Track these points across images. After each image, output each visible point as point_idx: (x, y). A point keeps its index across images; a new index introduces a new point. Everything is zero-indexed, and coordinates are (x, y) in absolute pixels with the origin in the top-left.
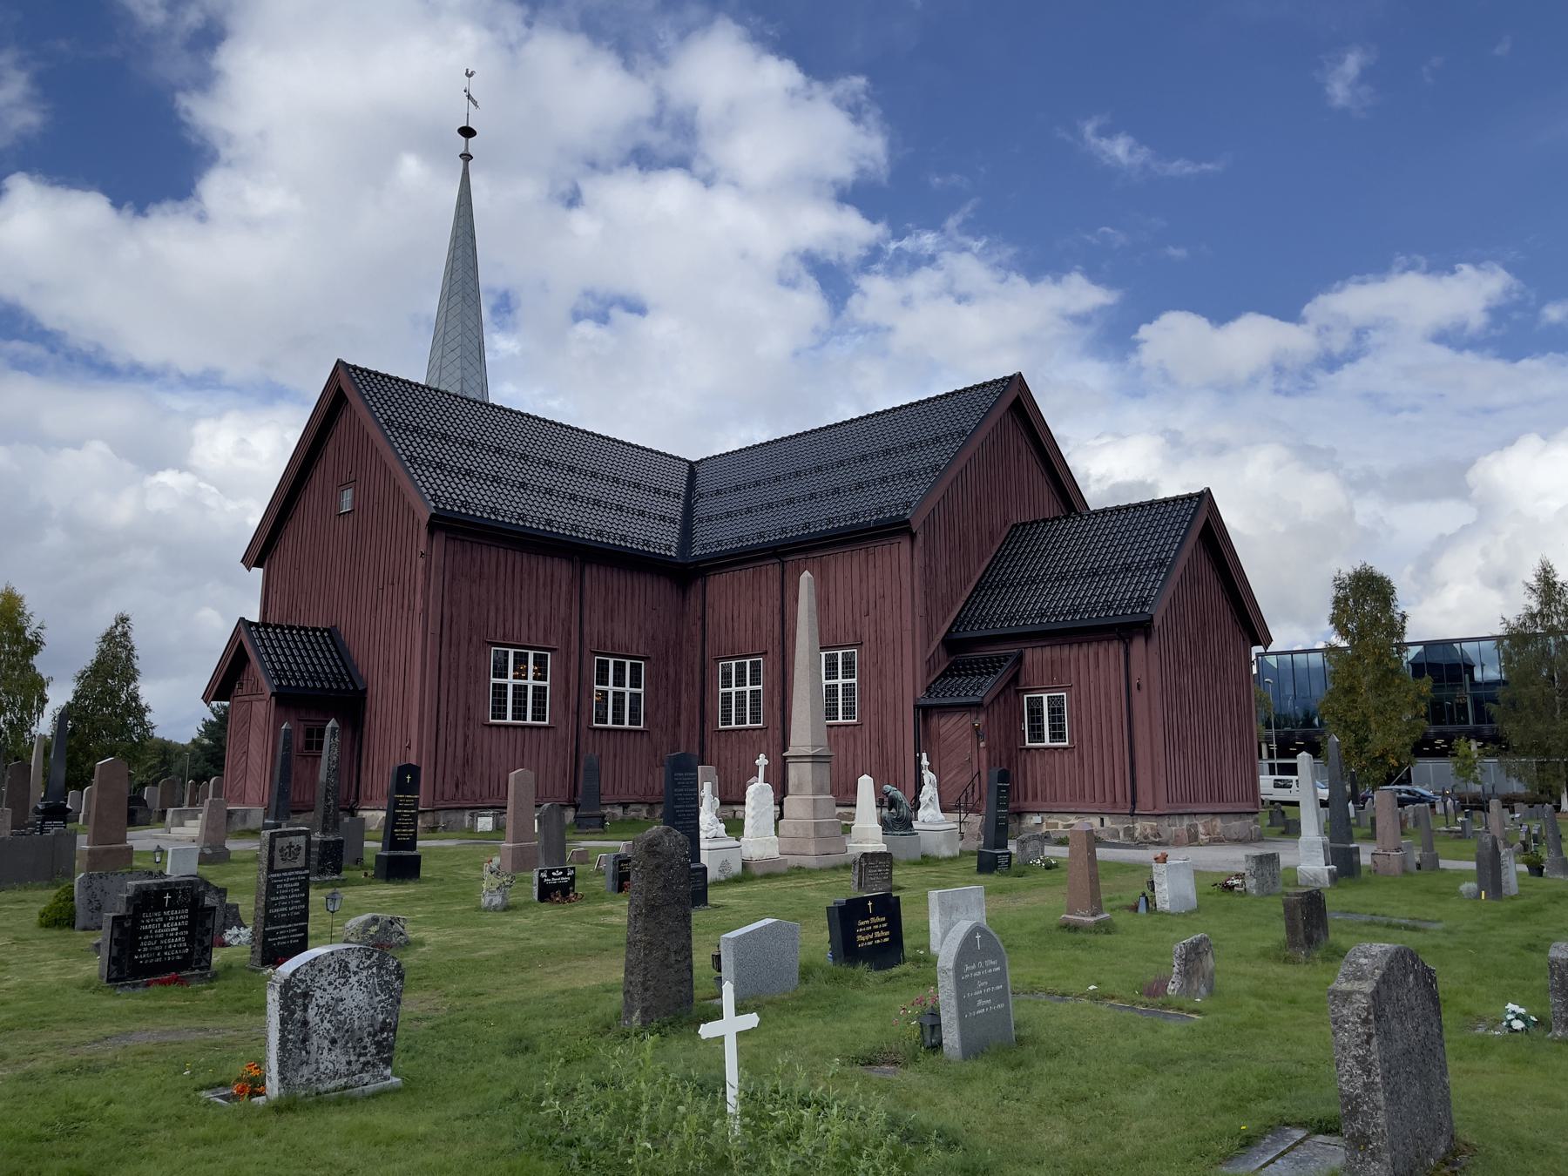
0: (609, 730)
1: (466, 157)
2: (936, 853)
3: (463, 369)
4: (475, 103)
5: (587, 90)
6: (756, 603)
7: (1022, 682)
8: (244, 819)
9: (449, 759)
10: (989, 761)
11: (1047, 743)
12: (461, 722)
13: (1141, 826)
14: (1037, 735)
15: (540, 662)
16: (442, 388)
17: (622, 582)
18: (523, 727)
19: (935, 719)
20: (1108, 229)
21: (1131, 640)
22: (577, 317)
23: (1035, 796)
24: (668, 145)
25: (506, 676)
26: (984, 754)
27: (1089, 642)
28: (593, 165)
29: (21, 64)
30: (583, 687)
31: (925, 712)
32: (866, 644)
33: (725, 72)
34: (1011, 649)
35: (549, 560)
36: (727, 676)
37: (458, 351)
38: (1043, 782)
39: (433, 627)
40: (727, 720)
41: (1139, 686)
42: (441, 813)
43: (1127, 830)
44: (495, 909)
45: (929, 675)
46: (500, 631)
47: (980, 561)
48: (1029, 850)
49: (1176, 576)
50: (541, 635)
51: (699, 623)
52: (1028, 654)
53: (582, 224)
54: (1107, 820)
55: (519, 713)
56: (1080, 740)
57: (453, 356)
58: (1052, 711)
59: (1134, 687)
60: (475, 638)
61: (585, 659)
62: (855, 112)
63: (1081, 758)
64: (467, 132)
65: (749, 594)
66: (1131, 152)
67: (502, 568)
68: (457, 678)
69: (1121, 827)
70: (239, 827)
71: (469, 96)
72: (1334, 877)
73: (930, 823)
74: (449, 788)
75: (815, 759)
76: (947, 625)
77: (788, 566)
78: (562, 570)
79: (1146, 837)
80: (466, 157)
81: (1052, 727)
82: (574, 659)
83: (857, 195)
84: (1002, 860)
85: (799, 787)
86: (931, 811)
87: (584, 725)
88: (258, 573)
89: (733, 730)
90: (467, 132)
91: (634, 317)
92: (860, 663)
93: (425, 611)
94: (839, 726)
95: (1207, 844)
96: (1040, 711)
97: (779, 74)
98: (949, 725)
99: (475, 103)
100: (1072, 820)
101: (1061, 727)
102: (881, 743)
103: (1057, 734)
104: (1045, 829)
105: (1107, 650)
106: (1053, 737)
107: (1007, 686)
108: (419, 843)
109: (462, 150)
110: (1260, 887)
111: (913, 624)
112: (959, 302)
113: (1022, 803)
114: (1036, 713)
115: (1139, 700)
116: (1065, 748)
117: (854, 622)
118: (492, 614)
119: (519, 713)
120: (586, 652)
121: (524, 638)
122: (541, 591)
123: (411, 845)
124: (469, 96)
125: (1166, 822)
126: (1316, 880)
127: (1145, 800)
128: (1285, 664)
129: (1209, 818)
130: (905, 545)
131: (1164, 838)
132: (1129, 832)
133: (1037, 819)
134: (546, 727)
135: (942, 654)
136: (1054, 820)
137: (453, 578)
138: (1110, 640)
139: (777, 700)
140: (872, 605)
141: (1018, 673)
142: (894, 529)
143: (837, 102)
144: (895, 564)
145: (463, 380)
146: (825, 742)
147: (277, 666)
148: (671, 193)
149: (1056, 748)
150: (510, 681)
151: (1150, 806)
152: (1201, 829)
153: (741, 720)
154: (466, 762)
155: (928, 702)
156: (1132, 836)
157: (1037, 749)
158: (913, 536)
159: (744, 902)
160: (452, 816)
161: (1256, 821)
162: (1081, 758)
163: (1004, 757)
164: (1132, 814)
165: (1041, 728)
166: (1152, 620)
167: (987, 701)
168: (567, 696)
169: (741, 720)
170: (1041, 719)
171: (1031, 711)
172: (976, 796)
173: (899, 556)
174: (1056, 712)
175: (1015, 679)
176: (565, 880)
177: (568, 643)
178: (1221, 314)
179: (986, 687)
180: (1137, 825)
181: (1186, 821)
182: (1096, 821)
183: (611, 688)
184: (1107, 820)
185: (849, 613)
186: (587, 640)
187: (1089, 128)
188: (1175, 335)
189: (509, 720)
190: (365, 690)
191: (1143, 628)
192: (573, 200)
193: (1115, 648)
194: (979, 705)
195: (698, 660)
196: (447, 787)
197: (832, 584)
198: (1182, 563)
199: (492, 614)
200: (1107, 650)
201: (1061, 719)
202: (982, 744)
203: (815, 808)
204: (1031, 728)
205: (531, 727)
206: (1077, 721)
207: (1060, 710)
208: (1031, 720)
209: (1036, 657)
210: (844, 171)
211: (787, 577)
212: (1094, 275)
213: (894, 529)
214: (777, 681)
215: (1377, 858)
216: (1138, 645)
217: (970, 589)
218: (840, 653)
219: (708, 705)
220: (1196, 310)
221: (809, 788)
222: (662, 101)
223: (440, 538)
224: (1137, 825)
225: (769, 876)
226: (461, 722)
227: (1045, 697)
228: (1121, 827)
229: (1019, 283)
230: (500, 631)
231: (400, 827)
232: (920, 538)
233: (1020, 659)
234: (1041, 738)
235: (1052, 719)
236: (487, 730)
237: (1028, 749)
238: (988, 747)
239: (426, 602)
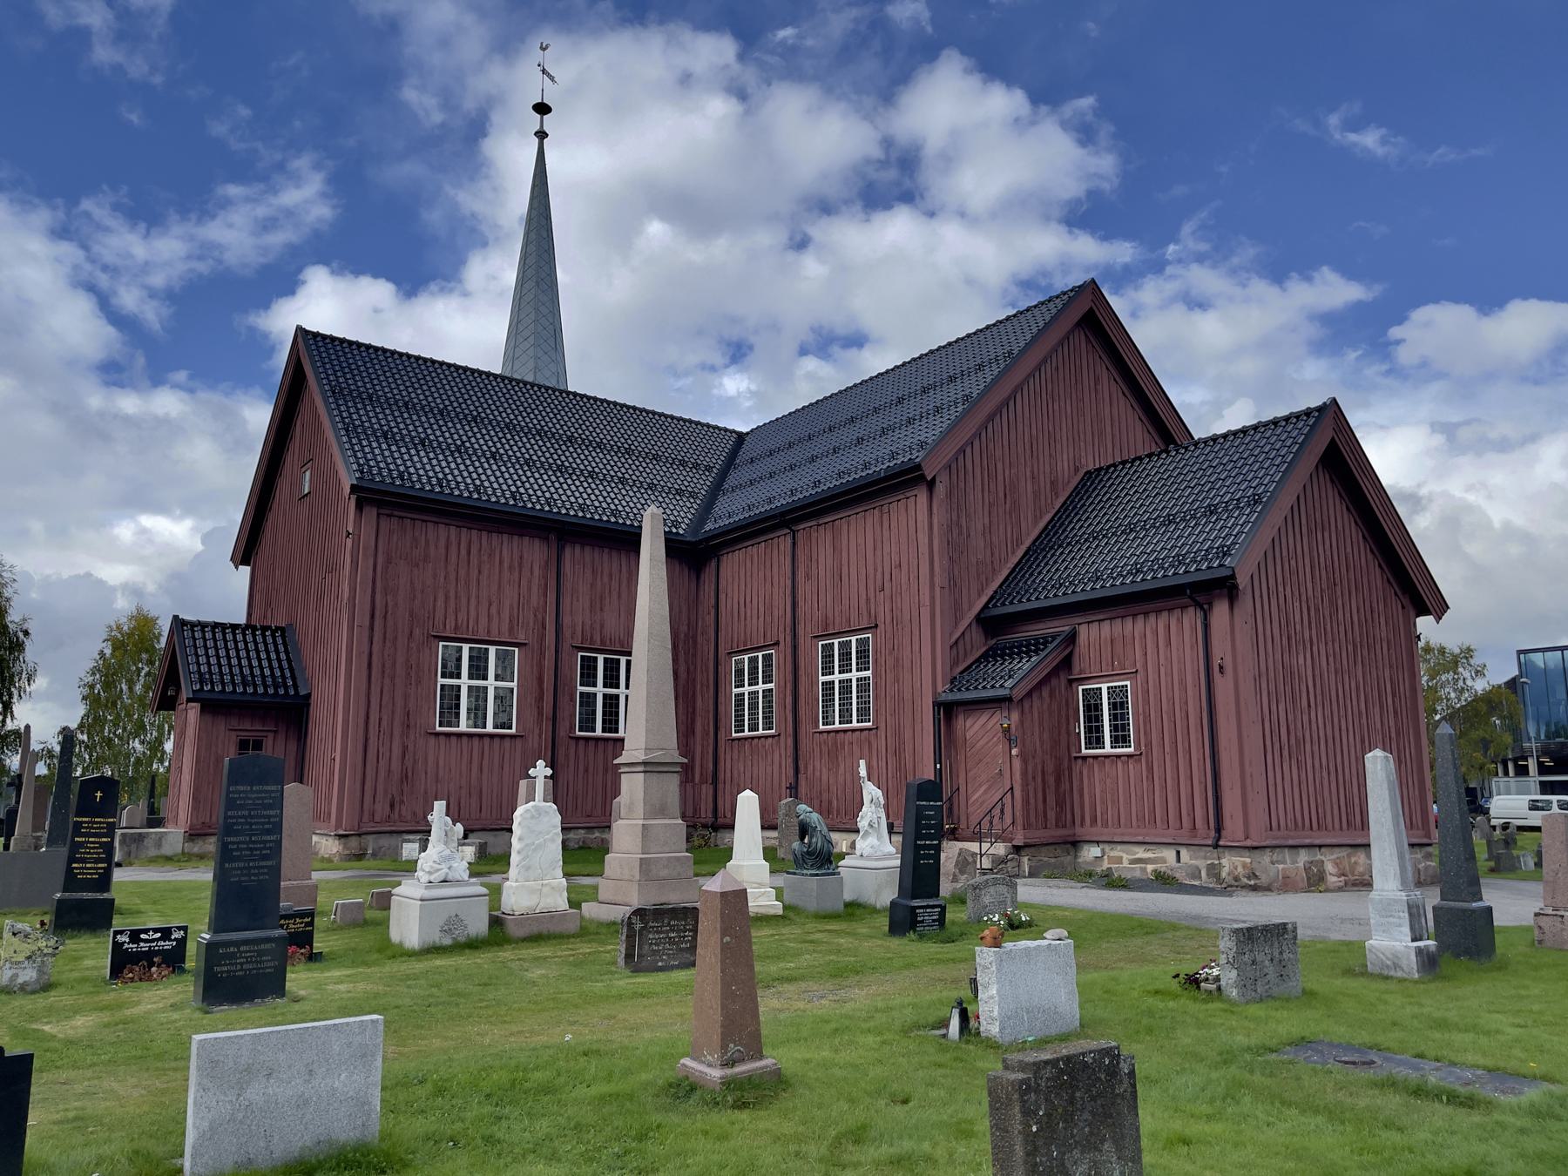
0: (597, 739)
1: (542, 135)
2: (872, 901)
3: (537, 358)
4: (552, 78)
5: (820, 135)
6: (768, 585)
7: (1076, 669)
8: (159, 844)
9: (382, 774)
10: (1024, 773)
11: (1108, 749)
12: (397, 732)
13: (1232, 863)
14: (1095, 739)
15: (503, 659)
16: (516, 376)
17: (615, 565)
18: (481, 736)
19: (961, 718)
20: (1362, 224)
21: (1210, 604)
22: (803, 351)
23: (1094, 821)
24: (894, 181)
25: (459, 676)
26: (1017, 764)
27: (1158, 611)
28: (826, 208)
29: (317, 167)
30: (560, 686)
31: (947, 711)
32: (881, 626)
33: (950, 105)
34: (1061, 626)
35: (614, 554)
36: (740, 672)
37: (531, 340)
38: (1104, 802)
39: (362, 618)
40: (740, 729)
41: (1221, 667)
42: (370, 838)
43: (1211, 867)
44: (23, 988)
45: (955, 663)
46: (450, 624)
47: (1036, 523)
48: (987, 900)
49: (1276, 517)
50: (505, 627)
51: (713, 612)
52: (1083, 631)
53: (812, 267)
54: (1184, 852)
55: (477, 713)
56: (1149, 744)
57: (527, 344)
58: (1113, 706)
59: (1216, 669)
60: (417, 631)
61: (564, 656)
62: (1085, 134)
63: (1150, 769)
64: (542, 109)
65: (761, 574)
66: (1384, 141)
67: (454, 549)
68: (393, 678)
69: (1202, 864)
70: (153, 852)
71: (544, 71)
72: (1429, 962)
73: (869, 858)
74: (381, 808)
75: (649, 767)
76: (984, 599)
77: (799, 535)
78: (535, 552)
79: (1236, 879)
80: (542, 135)
81: (1114, 728)
82: (550, 654)
83: (1085, 215)
84: (927, 916)
85: (630, 808)
86: (872, 840)
87: (562, 732)
88: (246, 570)
89: (746, 739)
90: (542, 109)
91: (853, 352)
92: (876, 652)
93: (352, 598)
94: (853, 731)
95: (1340, 889)
96: (1098, 707)
97: (1003, 102)
98: (977, 727)
99: (552, 78)
100: (1141, 853)
101: (1125, 727)
102: (898, 753)
103: (1120, 739)
104: (1106, 865)
105: (1180, 621)
106: (1116, 741)
107: (1054, 672)
108: (118, 875)
109: (537, 128)
110: (1242, 985)
111: (932, 598)
112: (1191, 309)
113: (1078, 830)
114: (1093, 709)
115: (1223, 686)
116: (1130, 756)
117: (868, 600)
118: (440, 603)
119: (477, 713)
120: (566, 646)
121: (495, 631)
122: (506, 574)
123: (104, 882)
124: (544, 71)
125: (1266, 858)
126: (1396, 966)
127: (1233, 825)
128: (1551, 665)
129: (1343, 853)
130: (922, 495)
131: (1264, 880)
132: (1214, 871)
133: (1095, 851)
134: (512, 736)
135: (977, 635)
136: (1117, 852)
137: (389, 561)
138: (1183, 608)
139: (789, 700)
140: (887, 577)
141: (1070, 655)
142: (906, 479)
143: (1065, 125)
144: (912, 523)
145: (536, 369)
146: (672, 742)
147: (204, 669)
148: (897, 229)
149: (1119, 756)
150: (464, 682)
151: (1240, 834)
152: (1330, 867)
153: (754, 727)
154: (405, 777)
155: (951, 697)
156: (1217, 876)
157: (1095, 757)
158: (931, 485)
159: (176, 1016)
160: (385, 841)
161: (1428, 856)
162: (1150, 769)
163: (1050, 768)
164: (1216, 846)
165: (1100, 729)
166: (1233, 577)
167: (1018, 694)
168: (540, 698)
169: (754, 727)
170: (1099, 718)
171: (1088, 708)
172: (1008, 820)
173: (913, 517)
174: (1118, 707)
175: (1066, 664)
176: (167, 945)
177: (542, 637)
178: (1489, 300)
179: (1018, 673)
180: (1224, 861)
181: (1303, 857)
182: (1169, 854)
183: (464, 682)
184: (1184, 852)
185: (862, 588)
186: (567, 633)
187: (1334, 120)
188: (1438, 327)
189: (599, 732)
190: (309, 696)
191: (1226, 587)
192: (801, 244)
193: (1191, 618)
194: (1008, 699)
195: (712, 656)
196: (378, 807)
197: (845, 554)
198: (1287, 500)
199: (440, 603)
200: (1180, 621)
201: (1124, 716)
202: (1014, 752)
203: (644, 836)
204: (1089, 730)
205: (492, 736)
206: (1145, 719)
207: (1123, 705)
208: (1088, 719)
209: (1093, 635)
210: (1072, 188)
211: (799, 552)
212: (1350, 272)
213: (906, 479)
214: (790, 677)
215: (1544, 922)
216: (1220, 610)
217: (1020, 553)
218: (854, 639)
219: (721, 708)
220: (1457, 298)
221: (640, 809)
222: (887, 143)
223: (371, 513)
224: (1224, 861)
225: (536, 939)
226: (397, 732)
227: (1104, 687)
228: (1202, 864)
229: (1260, 287)
230: (450, 624)
231: (83, 861)
232: (940, 489)
233: (1072, 638)
234: (1099, 742)
235: (1113, 717)
236: (432, 740)
237: (1085, 758)
238: (1021, 755)
239: (353, 590)
